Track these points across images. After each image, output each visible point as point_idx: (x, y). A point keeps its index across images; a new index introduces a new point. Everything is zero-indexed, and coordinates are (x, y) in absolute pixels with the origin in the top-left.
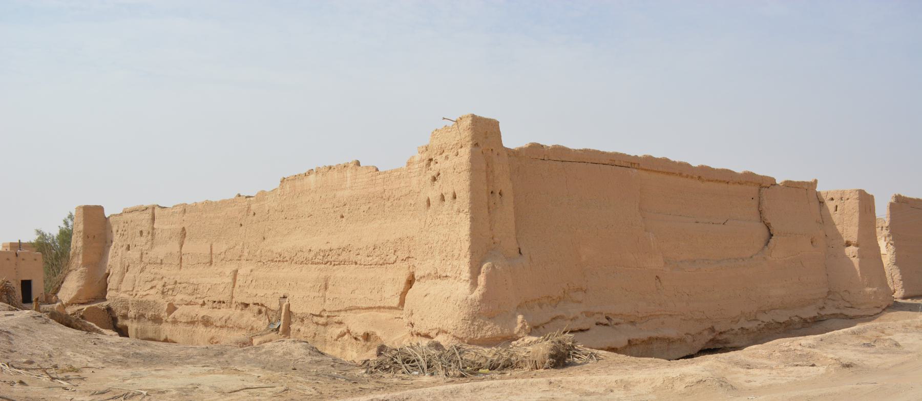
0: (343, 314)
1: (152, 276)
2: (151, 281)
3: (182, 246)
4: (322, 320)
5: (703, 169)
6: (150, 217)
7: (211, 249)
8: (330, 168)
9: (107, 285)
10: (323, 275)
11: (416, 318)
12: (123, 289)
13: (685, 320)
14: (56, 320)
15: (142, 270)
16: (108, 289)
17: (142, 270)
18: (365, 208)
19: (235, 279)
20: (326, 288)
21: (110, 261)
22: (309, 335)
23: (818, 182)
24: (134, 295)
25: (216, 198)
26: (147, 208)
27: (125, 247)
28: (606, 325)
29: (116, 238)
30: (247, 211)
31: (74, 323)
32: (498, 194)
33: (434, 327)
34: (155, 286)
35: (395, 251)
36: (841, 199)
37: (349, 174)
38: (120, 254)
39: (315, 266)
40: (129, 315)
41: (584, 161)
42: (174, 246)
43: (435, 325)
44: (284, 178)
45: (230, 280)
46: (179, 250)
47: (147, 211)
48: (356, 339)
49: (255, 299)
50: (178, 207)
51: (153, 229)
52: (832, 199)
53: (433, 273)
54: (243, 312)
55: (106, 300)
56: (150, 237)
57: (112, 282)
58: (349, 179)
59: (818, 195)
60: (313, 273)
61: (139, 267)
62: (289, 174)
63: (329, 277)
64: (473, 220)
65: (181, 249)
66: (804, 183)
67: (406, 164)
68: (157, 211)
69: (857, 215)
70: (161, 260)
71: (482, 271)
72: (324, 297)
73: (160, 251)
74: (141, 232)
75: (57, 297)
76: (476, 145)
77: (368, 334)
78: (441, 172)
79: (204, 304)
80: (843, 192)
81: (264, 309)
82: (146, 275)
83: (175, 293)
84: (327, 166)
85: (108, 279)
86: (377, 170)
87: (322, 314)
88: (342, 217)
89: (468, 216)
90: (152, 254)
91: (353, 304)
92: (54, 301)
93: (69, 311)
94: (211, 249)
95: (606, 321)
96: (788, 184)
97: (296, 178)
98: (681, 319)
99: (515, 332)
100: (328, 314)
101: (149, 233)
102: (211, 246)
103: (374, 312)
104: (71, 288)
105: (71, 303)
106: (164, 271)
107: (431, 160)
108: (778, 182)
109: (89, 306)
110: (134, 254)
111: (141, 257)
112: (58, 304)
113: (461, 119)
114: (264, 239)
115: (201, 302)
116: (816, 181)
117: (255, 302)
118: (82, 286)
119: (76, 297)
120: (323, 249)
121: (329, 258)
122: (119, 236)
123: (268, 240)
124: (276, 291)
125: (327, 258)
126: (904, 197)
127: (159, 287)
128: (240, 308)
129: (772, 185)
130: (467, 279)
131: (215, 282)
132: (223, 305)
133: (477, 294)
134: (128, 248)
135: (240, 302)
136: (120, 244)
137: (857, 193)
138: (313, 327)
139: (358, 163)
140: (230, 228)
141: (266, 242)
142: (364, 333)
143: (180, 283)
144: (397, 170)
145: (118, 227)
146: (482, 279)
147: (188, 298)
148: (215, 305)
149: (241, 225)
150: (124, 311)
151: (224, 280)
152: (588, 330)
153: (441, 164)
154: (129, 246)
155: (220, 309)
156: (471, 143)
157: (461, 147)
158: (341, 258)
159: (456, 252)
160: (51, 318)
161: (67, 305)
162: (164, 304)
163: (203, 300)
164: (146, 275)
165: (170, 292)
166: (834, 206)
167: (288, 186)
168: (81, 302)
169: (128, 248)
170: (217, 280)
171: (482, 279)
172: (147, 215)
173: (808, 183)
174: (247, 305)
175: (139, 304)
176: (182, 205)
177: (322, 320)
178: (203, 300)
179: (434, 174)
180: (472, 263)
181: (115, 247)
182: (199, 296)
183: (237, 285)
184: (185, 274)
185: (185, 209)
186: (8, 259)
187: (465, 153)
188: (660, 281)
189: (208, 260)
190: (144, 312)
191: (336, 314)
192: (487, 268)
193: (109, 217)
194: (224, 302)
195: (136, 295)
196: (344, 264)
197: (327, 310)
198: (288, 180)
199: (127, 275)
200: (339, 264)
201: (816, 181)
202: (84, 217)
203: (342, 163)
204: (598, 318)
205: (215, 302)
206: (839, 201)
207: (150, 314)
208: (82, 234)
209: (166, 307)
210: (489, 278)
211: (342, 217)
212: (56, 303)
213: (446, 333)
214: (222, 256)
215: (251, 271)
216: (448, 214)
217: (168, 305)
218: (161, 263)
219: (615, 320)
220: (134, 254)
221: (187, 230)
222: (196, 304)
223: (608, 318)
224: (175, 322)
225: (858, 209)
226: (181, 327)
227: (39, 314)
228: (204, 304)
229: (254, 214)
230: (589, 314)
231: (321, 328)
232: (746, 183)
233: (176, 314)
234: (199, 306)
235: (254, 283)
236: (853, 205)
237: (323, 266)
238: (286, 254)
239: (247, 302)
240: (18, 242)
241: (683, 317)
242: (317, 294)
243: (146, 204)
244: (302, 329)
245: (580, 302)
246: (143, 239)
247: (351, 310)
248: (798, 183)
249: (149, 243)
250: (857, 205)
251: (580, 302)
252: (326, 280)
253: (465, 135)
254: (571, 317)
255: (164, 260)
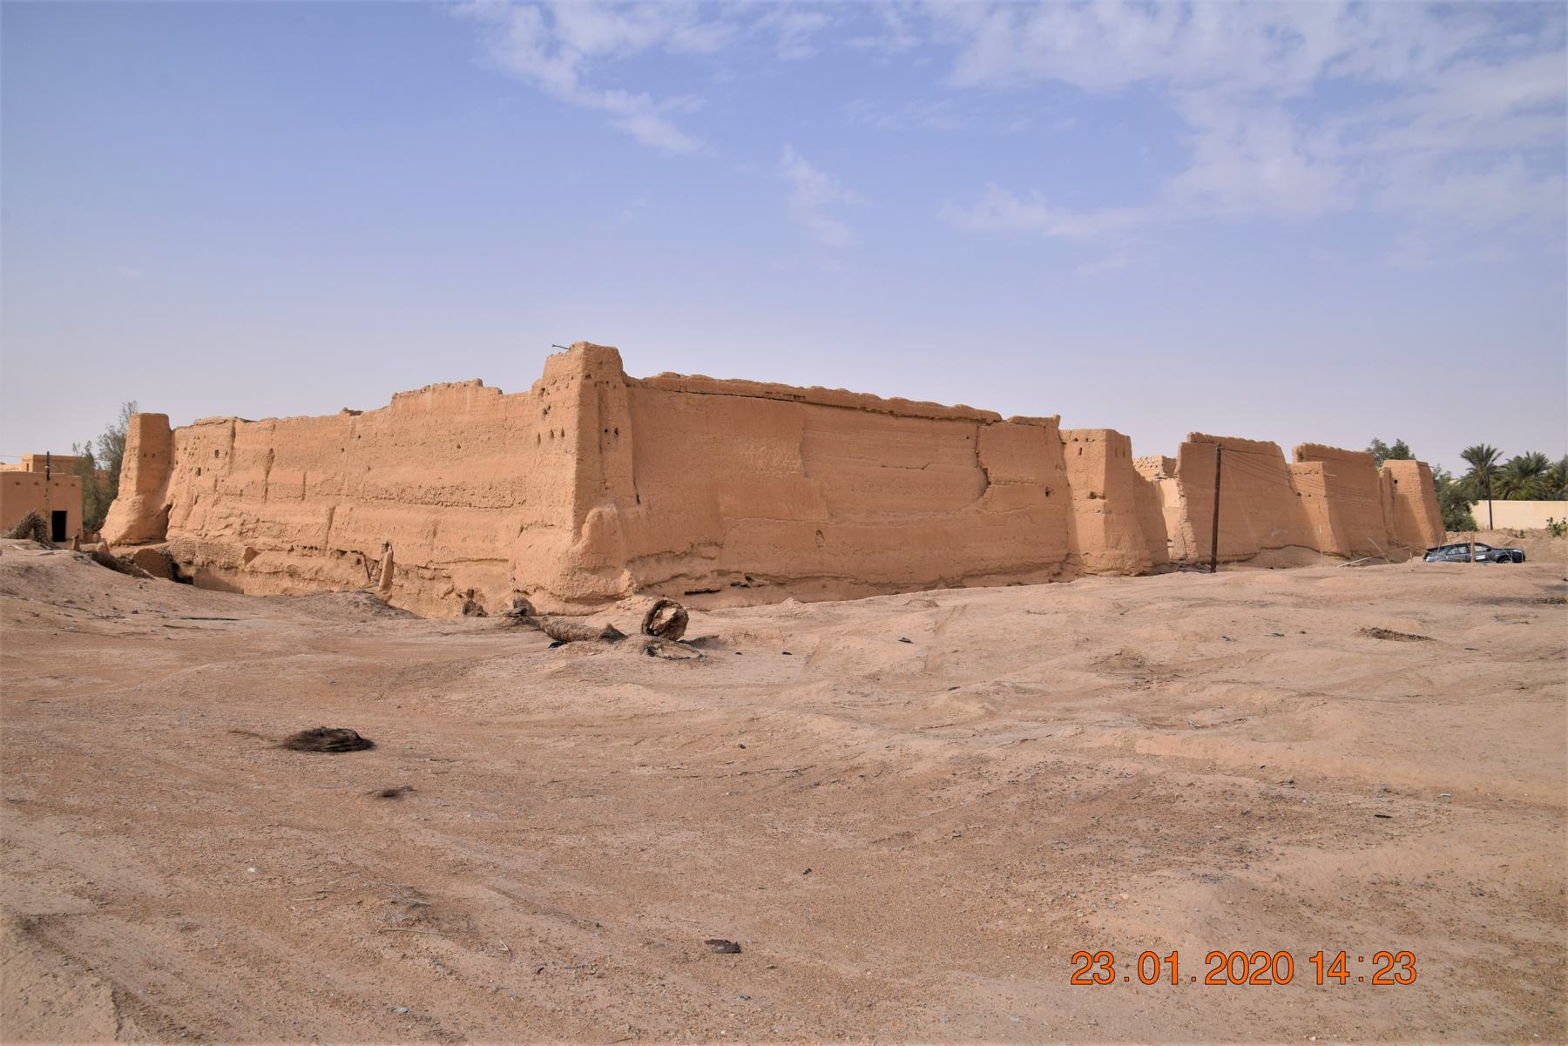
0: (452, 566)
1: (229, 512)
2: (227, 518)
3: (268, 472)
4: (428, 574)
5: (896, 401)
6: (230, 433)
7: (305, 479)
8: (449, 386)
9: (168, 521)
10: (433, 517)
11: (517, 573)
12: (189, 527)
13: (855, 584)
14: (98, 562)
15: (216, 503)
16: (169, 526)
17: (216, 503)
18: (485, 438)
19: (331, 520)
20: (435, 534)
21: (172, 488)
22: (413, 591)
23: (1062, 418)
24: (204, 535)
25: (314, 413)
26: (225, 421)
27: (194, 471)
28: (745, 586)
29: (180, 456)
30: (351, 433)
31: (118, 565)
32: (612, 433)
33: (533, 583)
34: (231, 525)
35: (512, 493)
36: (1087, 440)
37: (468, 394)
38: (187, 481)
39: (424, 506)
40: (195, 562)
41: (731, 392)
42: (258, 473)
43: (534, 581)
44: (397, 394)
45: (324, 520)
46: (264, 478)
47: (226, 425)
48: (460, 596)
49: (353, 545)
50: (266, 422)
51: (233, 448)
52: (1076, 440)
53: (539, 521)
54: (339, 561)
55: (166, 541)
56: (228, 459)
57: (175, 518)
58: (468, 401)
59: (1059, 432)
60: (421, 516)
61: (211, 499)
62: (402, 389)
63: (439, 522)
64: (580, 461)
65: (267, 477)
66: (1040, 419)
67: (531, 388)
68: (239, 425)
69: (1103, 460)
70: (241, 491)
71: (587, 520)
72: (431, 544)
73: (240, 479)
74: (217, 452)
75: (99, 534)
76: (588, 376)
77: (473, 591)
78: (552, 405)
79: (292, 550)
80: (1089, 432)
81: (362, 559)
82: (221, 509)
83: (256, 534)
84: (446, 382)
85: (170, 513)
86: (500, 392)
87: (429, 566)
88: (459, 447)
89: (575, 458)
90: (228, 481)
91: (463, 555)
92: (95, 540)
93: (116, 553)
94: (305, 479)
95: (744, 582)
96: (1019, 421)
97: (410, 395)
98: (850, 583)
99: (621, 591)
100: (436, 566)
101: (227, 453)
102: (305, 475)
103: (485, 566)
104: (118, 521)
105: (119, 544)
106: (243, 506)
107: (544, 389)
108: (1004, 418)
109: (141, 548)
110: (206, 481)
111: (216, 486)
112: (100, 544)
113: (574, 346)
114: (369, 469)
115: (288, 547)
116: (1058, 418)
117: (354, 550)
118: (134, 521)
119: (125, 537)
120: (433, 486)
121: (443, 499)
122: (187, 455)
123: (373, 472)
124: (378, 536)
125: (437, 499)
126: (1207, 436)
127: (237, 526)
128: (336, 556)
129: (995, 421)
130: (571, 528)
131: (307, 523)
132: (316, 552)
133: (580, 546)
134: (199, 472)
135: (335, 548)
136: (188, 467)
137: (1105, 433)
138: (418, 583)
139: (480, 383)
140: (328, 453)
141: (371, 473)
142: (469, 590)
143: (263, 522)
144: (520, 395)
145: (187, 443)
146: (586, 529)
147: (272, 542)
148: (305, 552)
149: (343, 450)
150: (188, 557)
151: (317, 520)
152: (718, 591)
153: (554, 397)
154: (200, 469)
155: (311, 556)
156: (582, 374)
157: (573, 378)
158: (454, 498)
159: (562, 498)
160: (93, 559)
161: (112, 545)
162: (240, 548)
163: (290, 545)
164: (221, 509)
165: (250, 533)
166: (1078, 448)
167: (400, 404)
168: (132, 542)
169: (199, 472)
170: (310, 520)
171: (586, 529)
172: (226, 430)
173: (1046, 420)
174: (344, 553)
175: (206, 546)
176: (271, 419)
177: (428, 574)
178: (290, 545)
179: (546, 407)
180: (576, 515)
181: (181, 471)
182: (286, 539)
183: (333, 528)
184: (272, 510)
185: (274, 425)
186: (36, 484)
187: (575, 386)
188: (822, 537)
189: (299, 493)
190: (214, 559)
191: (445, 566)
192: (593, 517)
193: (175, 430)
194: (316, 548)
195: (206, 535)
196: (457, 506)
197: (435, 561)
198: (401, 397)
199: (195, 508)
200: (452, 505)
201: (1058, 418)
202: (141, 428)
203: (463, 381)
204: (735, 578)
205: (305, 547)
206: (1084, 442)
207: (223, 561)
208: (136, 451)
209: (243, 553)
210: (594, 528)
211: (459, 447)
212: (97, 542)
213: (543, 589)
214: (318, 489)
215: (351, 509)
216: (556, 454)
217: (247, 550)
218: (241, 495)
219: (758, 581)
220: (206, 481)
221: (275, 452)
222: (282, 550)
223: (748, 579)
224: (253, 572)
225: (1104, 453)
226: (261, 578)
227: (79, 554)
228: (292, 550)
229: (359, 437)
230: (721, 573)
231: (427, 583)
232: (959, 419)
233: (257, 561)
234: (285, 553)
235: (353, 525)
236: (1099, 449)
237: (433, 506)
238: (393, 490)
239: (343, 549)
240: (46, 454)
241: (853, 580)
242: (424, 542)
243: (226, 416)
244: (406, 584)
245: (712, 559)
246: (219, 462)
247: (461, 561)
248: (1033, 419)
249: (226, 467)
250: (1104, 448)
251: (712, 559)
252: (436, 524)
253: (575, 366)
254: (698, 575)
255: (246, 490)
